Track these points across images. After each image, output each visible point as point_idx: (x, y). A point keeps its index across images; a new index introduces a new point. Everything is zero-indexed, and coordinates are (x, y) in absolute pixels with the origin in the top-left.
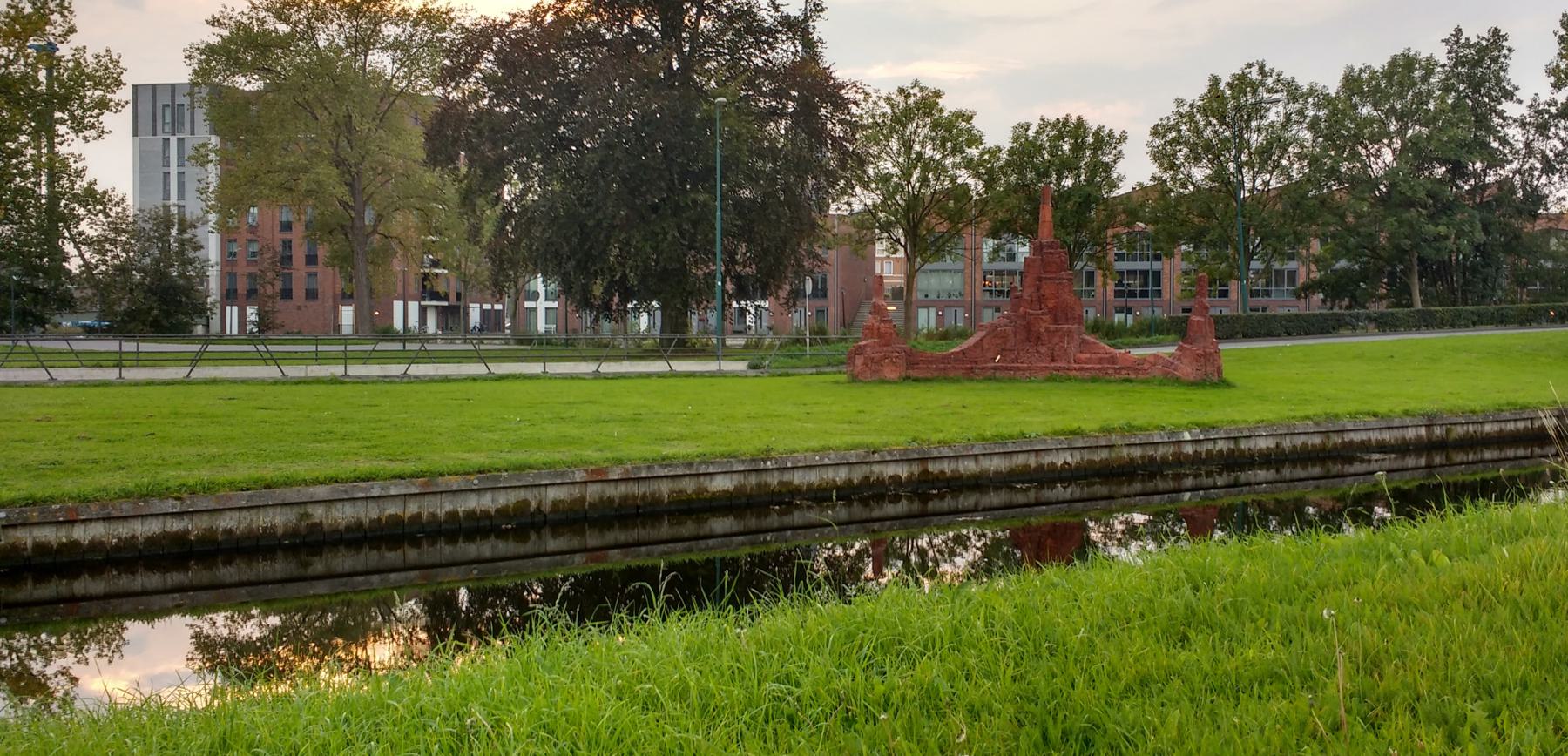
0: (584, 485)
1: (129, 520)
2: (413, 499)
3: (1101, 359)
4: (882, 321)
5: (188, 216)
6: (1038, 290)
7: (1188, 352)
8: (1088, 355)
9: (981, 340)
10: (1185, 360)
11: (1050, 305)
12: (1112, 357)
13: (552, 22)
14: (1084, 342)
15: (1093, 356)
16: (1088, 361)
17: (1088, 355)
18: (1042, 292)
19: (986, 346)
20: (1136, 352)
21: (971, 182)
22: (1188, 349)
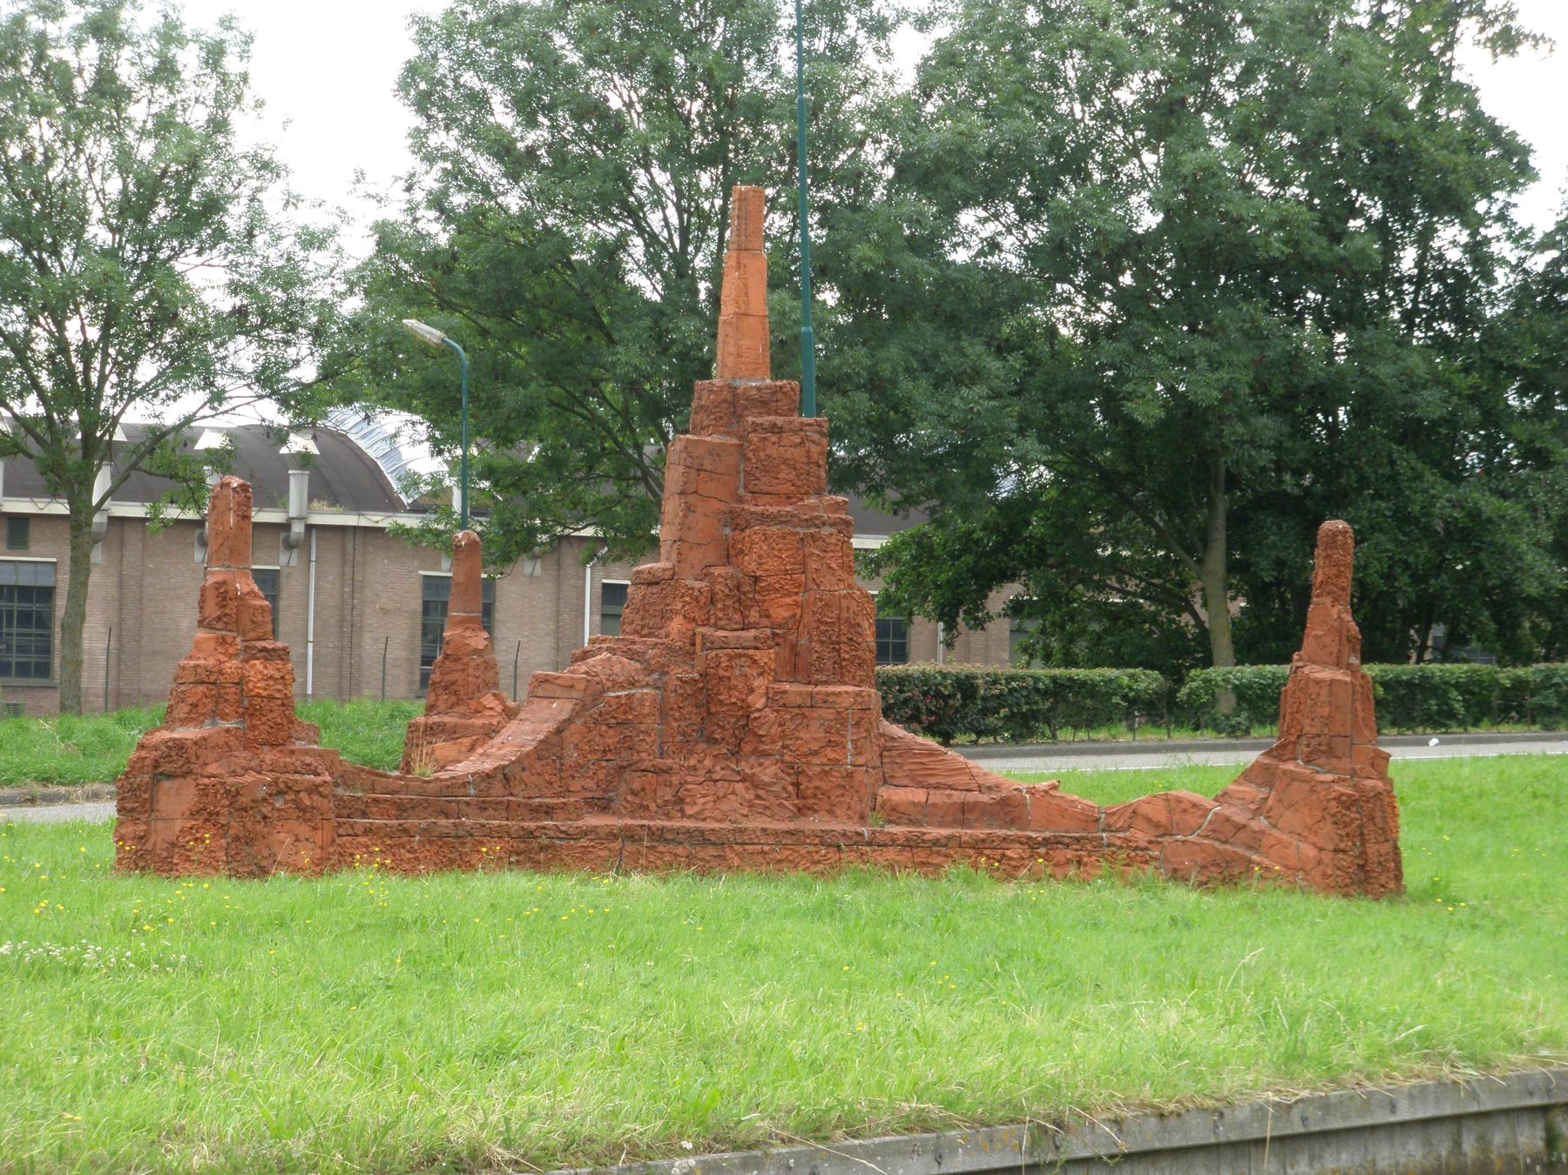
0: (1451, 1128)
1: (1397, 1133)
2: (1471, 1123)
3: (964, 808)
4: (250, 654)
5: (67, 535)
6: (729, 555)
7: (1297, 791)
8: (919, 795)
9: (559, 731)
10: (1292, 819)
11: (780, 613)
12: (1005, 802)
13: (1135, 423)
14: (887, 747)
15: (937, 797)
16: (926, 813)
17: (919, 795)
18: (750, 564)
19: (572, 756)
20: (985, 765)
21: (435, 228)
22: (1294, 777)
